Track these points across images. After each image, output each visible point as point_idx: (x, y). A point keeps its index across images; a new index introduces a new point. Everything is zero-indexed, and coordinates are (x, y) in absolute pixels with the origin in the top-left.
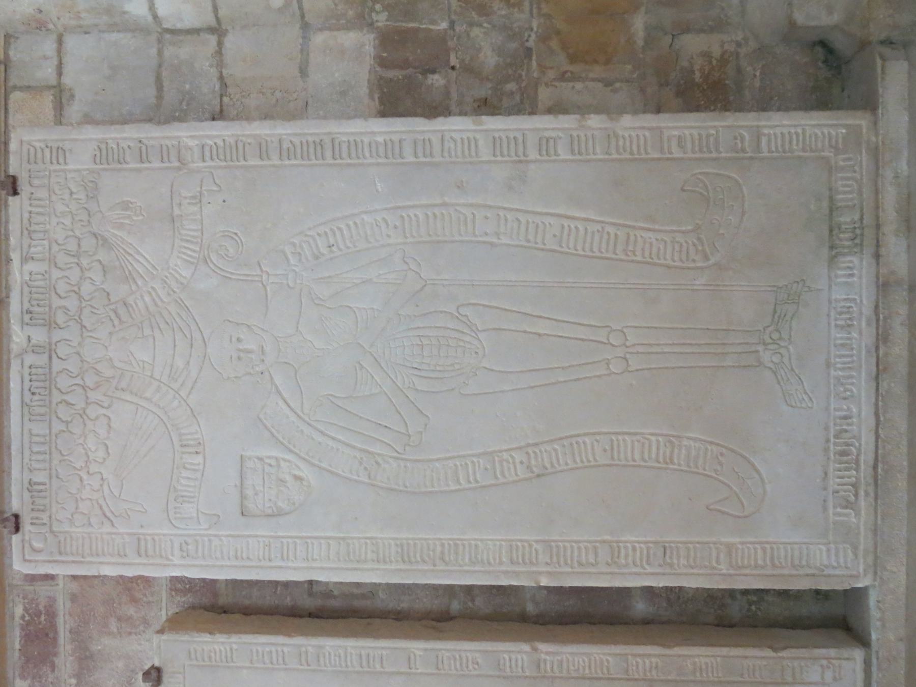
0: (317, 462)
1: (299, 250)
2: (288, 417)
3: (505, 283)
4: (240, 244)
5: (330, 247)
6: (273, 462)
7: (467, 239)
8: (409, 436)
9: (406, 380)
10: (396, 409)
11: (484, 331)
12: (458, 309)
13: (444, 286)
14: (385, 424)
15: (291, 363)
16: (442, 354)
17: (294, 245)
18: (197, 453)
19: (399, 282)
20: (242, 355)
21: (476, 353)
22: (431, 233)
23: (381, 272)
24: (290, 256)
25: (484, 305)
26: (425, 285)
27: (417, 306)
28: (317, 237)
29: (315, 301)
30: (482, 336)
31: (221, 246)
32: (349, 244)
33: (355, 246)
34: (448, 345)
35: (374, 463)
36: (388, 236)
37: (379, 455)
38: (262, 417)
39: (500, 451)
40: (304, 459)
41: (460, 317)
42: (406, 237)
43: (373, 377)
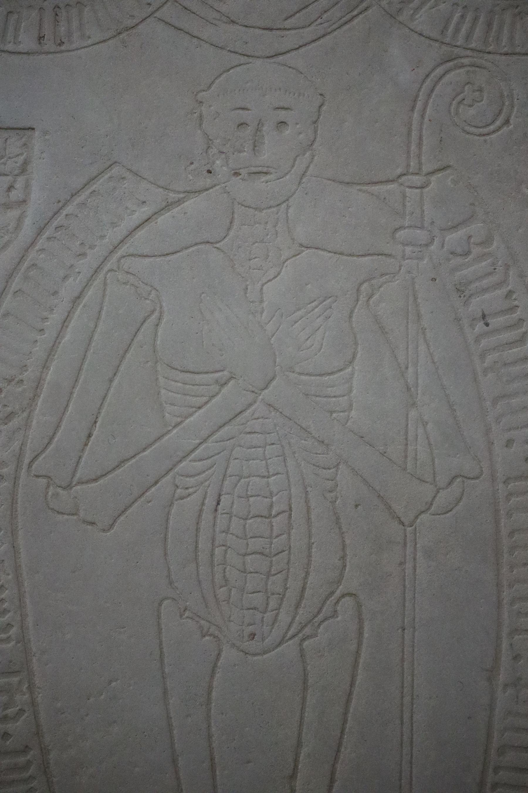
0: (14, 286)
1: (476, 251)
2: (114, 225)
3: (407, 699)
4: (485, 130)
5: (484, 316)
6: (15, 195)
7: (506, 615)
8: (68, 487)
9: (191, 481)
10: (128, 460)
11: (302, 650)
12: (350, 595)
13: (401, 564)
14: (95, 433)
15: (232, 233)
16: (248, 558)
17: (487, 241)
18: (41, 38)
19: (409, 465)
20: (249, 131)
21: (252, 636)
22: (516, 536)
23: (430, 426)
24: (461, 233)
25: (358, 653)
26: (403, 524)
27: (357, 506)
28: (504, 290)
29: (365, 285)
30: (292, 645)
31: (480, 90)
32: (490, 359)
33: (485, 371)
34: (269, 575)
35: (9, 409)
36: (509, 443)
37: (27, 424)
38: (115, 170)
39: (31, 688)
40: (22, 259)
41: (333, 598)
42: (506, 482)
43: (200, 408)
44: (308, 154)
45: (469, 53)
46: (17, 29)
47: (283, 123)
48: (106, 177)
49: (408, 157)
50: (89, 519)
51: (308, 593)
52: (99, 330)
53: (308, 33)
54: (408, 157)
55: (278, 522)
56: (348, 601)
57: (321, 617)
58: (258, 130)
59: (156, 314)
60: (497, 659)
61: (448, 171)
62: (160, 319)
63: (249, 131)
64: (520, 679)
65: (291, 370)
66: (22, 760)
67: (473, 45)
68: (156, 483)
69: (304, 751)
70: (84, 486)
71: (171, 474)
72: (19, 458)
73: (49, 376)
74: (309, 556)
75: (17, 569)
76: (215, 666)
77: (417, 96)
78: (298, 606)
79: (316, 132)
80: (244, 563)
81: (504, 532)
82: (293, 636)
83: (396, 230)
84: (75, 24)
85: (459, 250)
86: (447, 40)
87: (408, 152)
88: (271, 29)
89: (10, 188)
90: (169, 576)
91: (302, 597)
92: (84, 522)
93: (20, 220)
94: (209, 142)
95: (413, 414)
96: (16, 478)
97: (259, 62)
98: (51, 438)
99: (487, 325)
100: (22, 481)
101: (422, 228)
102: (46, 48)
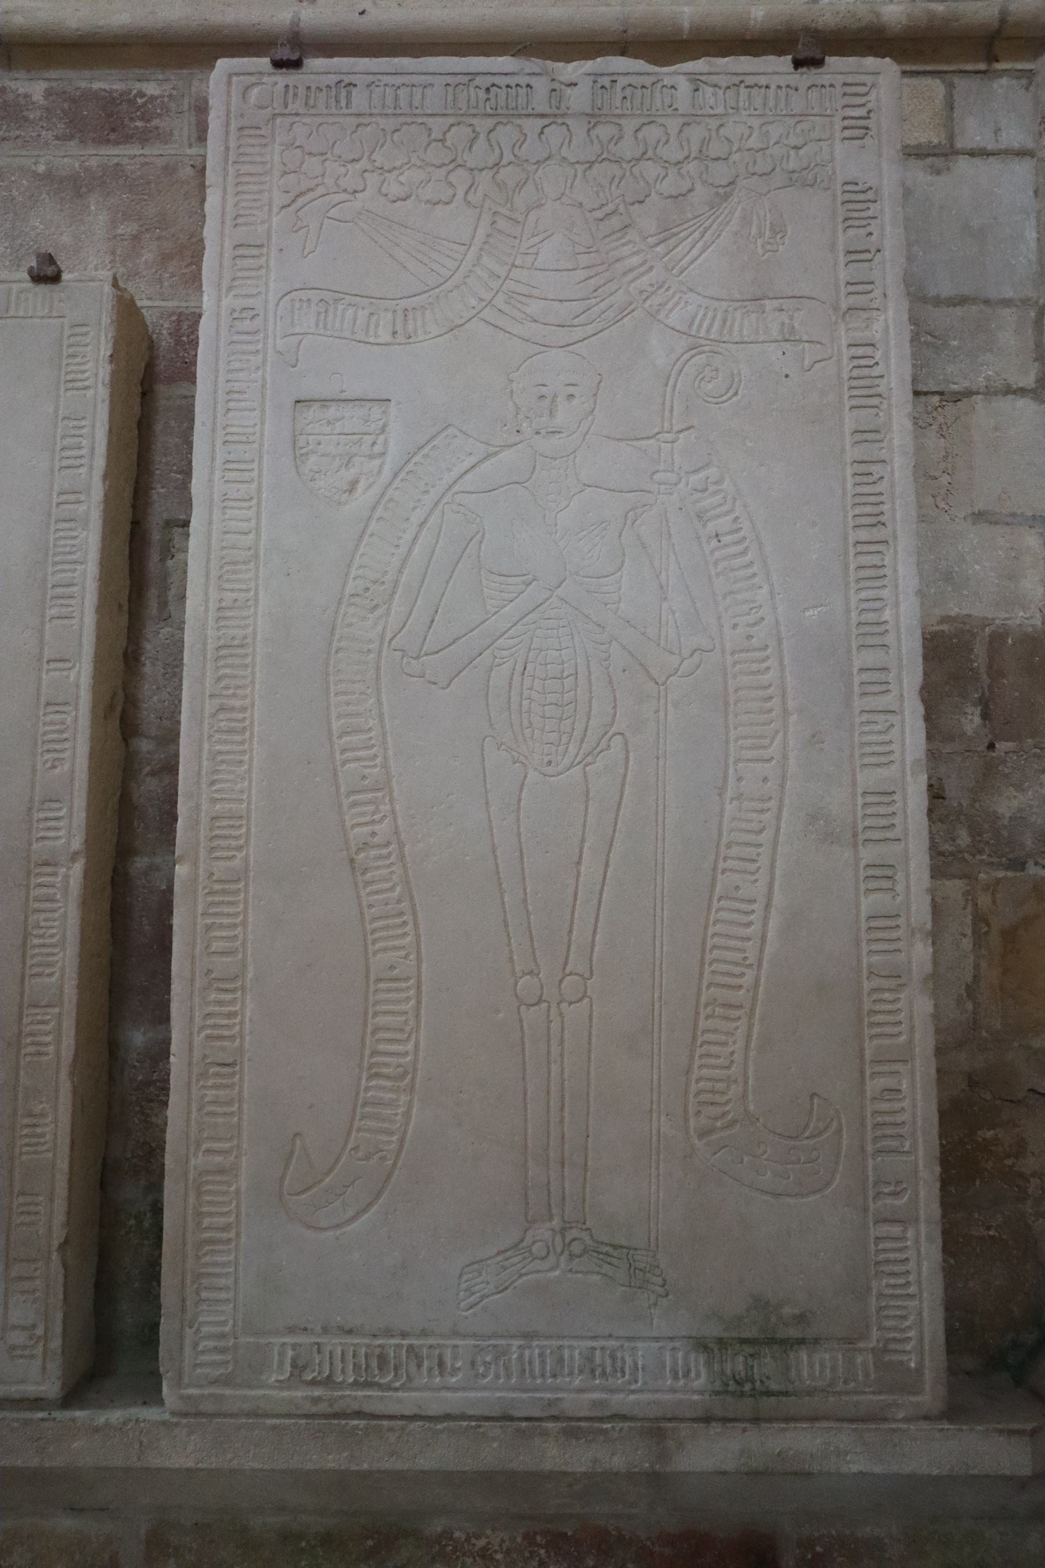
0: (378, 514)
1: (712, 488)
2: (449, 470)
4: (720, 400)
5: (717, 535)
6: (377, 449)
8: (417, 658)
9: (505, 653)
11: (585, 773)
15: (534, 477)
16: (546, 708)
20: (547, 401)
21: (550, 763)
23: (677, 615)
24: (701, 475)
25: (625, 776)
26: (657, 683)
28: (732, 516)
31: (717, 370)
32: (721, 566)
33: (718, 575)
34: (561, 719)
35: (375, 602)
38: (450, 431)
40: (383, 495)
42: (733, 653)
44: (590, 418)
45: (709, 342)
46: (377, 326)
47: (571, 396)
48: (444, 435)
49: (663, 421)
50: (433, 680)
51: (588, 733)
52: (439, 546)
53: (590, 329)
54: (663, 421)
55: (568, 682)
56: (618, 739)
57: (599, 749)
58: (553, 401)
59: (480, 534)
60: (725, 778)
61: (692, 431)
62: (483, 537)
63: (547, 401)
64: (742, 794)
65: (577, 574)
66: (385, 851)
67: (712, 337)
68: (480, 654)
69: (587, 845)
70: (430, 657)
71: (491, 648)
72: (382, 638)
73: (403, 580)
74: (590, 706)
75: (381, 716)
76: (523, 784)
77: (670, 375)
78: (582, 741)
79: (595, 402)
80: (544, 711)
81: (731, 690)
82: (580, 763)
83: (654, 473)
84: (419, 323)
85: (699, 487)
86: (693, 333)
87: (663, 416)
88: (563, 326)
89: (374, 443)
90: (490, 720)
91: (585, 735)
92: (429, 682)
93: (381, 466)
94: (518, 409)
95: (665, 605)
96: (380, 652)
97: (555, 350)
98: (405, 623)
99: (719, 541)
100: (384, 654)
101: (672, 471)
102: (398, 341)
